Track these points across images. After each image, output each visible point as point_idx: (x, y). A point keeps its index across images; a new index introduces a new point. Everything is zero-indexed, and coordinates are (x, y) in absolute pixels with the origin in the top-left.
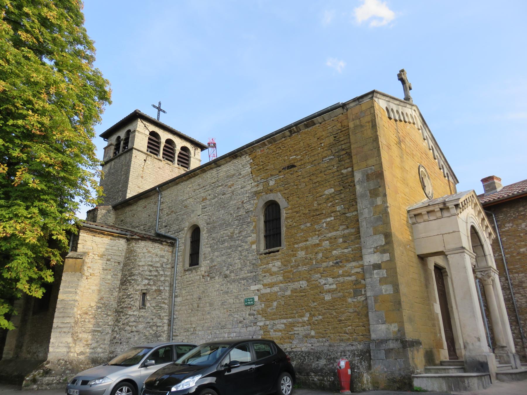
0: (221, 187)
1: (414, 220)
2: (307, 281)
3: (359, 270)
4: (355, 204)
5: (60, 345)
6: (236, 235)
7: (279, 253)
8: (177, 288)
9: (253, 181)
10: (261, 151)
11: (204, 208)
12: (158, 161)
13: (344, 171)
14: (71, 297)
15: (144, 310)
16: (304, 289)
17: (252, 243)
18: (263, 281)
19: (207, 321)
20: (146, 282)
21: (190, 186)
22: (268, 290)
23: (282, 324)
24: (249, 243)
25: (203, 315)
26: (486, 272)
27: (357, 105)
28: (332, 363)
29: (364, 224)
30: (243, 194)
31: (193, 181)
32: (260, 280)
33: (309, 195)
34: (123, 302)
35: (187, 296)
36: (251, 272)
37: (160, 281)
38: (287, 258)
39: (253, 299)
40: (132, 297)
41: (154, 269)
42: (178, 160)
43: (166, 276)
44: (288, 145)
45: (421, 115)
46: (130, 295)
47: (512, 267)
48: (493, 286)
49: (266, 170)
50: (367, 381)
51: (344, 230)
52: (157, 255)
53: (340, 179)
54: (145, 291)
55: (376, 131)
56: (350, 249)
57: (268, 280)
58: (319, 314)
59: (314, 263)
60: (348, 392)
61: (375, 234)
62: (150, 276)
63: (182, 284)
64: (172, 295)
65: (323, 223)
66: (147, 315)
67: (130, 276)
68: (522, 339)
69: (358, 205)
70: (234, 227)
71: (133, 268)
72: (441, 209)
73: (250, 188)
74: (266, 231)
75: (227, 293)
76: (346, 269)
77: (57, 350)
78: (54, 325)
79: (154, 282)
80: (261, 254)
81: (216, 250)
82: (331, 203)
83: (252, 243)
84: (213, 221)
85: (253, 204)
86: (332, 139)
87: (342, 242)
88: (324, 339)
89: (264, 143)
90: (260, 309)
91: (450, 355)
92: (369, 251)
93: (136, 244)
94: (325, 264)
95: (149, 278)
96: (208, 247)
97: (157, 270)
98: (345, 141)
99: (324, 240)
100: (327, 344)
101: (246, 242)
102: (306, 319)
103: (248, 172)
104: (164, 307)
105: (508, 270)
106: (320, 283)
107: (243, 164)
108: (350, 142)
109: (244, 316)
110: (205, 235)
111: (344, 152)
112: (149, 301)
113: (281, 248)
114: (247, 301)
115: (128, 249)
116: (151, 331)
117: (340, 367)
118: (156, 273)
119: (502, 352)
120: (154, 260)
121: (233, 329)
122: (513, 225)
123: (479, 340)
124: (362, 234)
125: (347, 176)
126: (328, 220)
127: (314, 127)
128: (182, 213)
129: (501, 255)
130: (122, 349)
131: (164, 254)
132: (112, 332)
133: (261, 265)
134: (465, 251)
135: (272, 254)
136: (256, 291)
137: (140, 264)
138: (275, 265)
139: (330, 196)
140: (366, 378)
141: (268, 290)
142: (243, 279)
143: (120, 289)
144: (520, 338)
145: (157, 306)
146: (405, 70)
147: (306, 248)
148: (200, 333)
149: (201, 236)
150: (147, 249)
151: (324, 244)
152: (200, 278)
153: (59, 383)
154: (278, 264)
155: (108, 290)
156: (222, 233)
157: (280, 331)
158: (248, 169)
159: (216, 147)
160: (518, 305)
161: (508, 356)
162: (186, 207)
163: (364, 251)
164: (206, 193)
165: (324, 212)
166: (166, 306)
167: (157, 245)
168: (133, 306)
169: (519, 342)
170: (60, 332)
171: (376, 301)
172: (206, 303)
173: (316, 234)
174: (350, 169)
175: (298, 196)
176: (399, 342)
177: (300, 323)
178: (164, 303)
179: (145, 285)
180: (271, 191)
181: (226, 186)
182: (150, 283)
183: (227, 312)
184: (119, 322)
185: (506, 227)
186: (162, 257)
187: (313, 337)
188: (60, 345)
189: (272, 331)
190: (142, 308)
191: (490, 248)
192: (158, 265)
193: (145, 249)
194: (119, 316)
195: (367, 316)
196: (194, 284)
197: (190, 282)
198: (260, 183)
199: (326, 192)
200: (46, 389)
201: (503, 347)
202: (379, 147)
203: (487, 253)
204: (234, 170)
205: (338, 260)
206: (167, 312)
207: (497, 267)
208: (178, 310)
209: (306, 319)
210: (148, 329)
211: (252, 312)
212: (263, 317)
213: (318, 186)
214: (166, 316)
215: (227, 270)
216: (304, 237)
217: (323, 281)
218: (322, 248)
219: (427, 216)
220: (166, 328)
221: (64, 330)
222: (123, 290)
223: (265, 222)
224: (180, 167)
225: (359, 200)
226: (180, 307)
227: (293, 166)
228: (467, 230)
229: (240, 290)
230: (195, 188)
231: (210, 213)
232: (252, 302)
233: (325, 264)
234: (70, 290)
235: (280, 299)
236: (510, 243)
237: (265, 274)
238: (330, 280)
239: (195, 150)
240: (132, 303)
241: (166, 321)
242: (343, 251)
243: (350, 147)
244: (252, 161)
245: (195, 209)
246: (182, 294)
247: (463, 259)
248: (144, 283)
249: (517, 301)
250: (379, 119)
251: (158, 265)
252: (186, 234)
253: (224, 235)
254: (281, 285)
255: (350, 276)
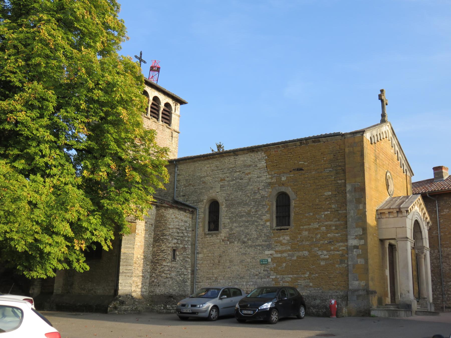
0: (238, 173)
1: (380, 216)
2: (308, 251)
3: (344, 248)
4: (345, 205)
5: (126, 284)
6: (253, 212)
7: (288, 230)
8: (199, 247)
9: (267, 174)
10: (275, 152)
11: (222, 187)
12: (147, 119)
13: (339, 182)
14: (130, 251)
15: (175, 263)
16: (306, 257)
17: (267, 221)
18: (275, 248)
19: (228, 273)
20: (176, 241)
21: (208, 166)
22: (279, 255)
23: (289, 278)
24: (264, 220)
25: (223, 268)
26: (421, 250)
27: (352, 136)
28: (324, 302)
29: (350, 220)
30: (259, 182)
31: (210, 162)
32: (272, 248)
33: (313, 193)
34: (158, 256)
35: (208, 254)
36: (266, 242)
37: (185, 241)
38: (294, 235)
39: (267, 260)
40: (165, 252)
41: (181, 231)
42: (162, 117)
43: (189, 237)
44: (298, 153)
45: (392, 128)
46: (163, 250)
47: (444, 243)
48: (425, 259)
49: (279, 167)
50: (345, 312)
51: (336, 221)
52: (182, 221)
53: (336, 187)
54: (175, 248)
55: (363, 159)
56: (340, 234)
57: (280, 248)
58: (316, 273)
59: (315, 240)
60: (335, 317)
61: (356, 227)
62: (178, 236)
63: (203, 244)
64: (194, 253)
65: (322, 215)
66: (177, 266)
67: (162, 236)
68: (442, 295)
69: (347, 207)
70: (251, 206)
71: (164, 230)
72: (397, 212)
73: (265, 179)
74: (277, 212)
75: (245, 254)
76: (336, 246)
77: (124, 288)
78: (121, 271)
79: (181, 241)
80: (274, 230)
81: (236, 222)
82: (328, 202)
83: (267, 221)
84: (232, 199)
85: (268, 192)
86: (332, 156)
87: (335, 229)
88: (319, 289)
89: (279, 146)
90: (273, 267)
91: (391, 302)
92: (352, 237)
93: (165, 210)
94: (322, 242)
95: (178, 238)
96: (227, 219)
97: (183, 233)
98: (342, 160)
99: (322, 226)
100: (320, 291)
101: (262, 220)
102: (307, 275)
103: (264, 166)
104: (188, 261)
105: (441, 244)
106: (317, 253)
107: (259, 158)
108: (345, 162)
109: (259, 271)
110: (224, 209)
111: (340, 168)
112: (178, 256)
113: (290, 227)
114: (262, 262)
115: (157, 214)
116: (180, 278)
117: (332, 304)
118: (182, 235)
119: (423, 301)
120: (180, 224)
121: (251, 280)
122: (449, 211)
123: (409, 292)
124: (348, 226)
125: (341, 185)
126: (326, 213)
127: (319, 143)
128: (201, 187)
129: (438, 233)
130: (160, 290)
131: (187, 220)
132: (150, 277)
133: (274, 238)
134: (408, 240)
135: (282, 231)
136: (270, 255)
137: (170, 227)
138: (285, 239)
139: (328, 197)
140: (345, 310)
141: (279, 255)
142: (259, 245)
143: (153, 245)
144: (441, 295)
145: (184, 259)
146: (384, 90)
147: (309, 230)
148: (221, 281)
149: (220, 209)
150: (175, 216)
151: (322, 229)
152: (220, 241)
153: (132, 310)
154: (288, 238)
155: (146, 246)
156: (240, 209)
157: (288, 282)
158: (263, 164)
159: (159, 72)
160: (444, 271)
161: (427, 304)
162: (204, 182)
163: (349, 237)
164: (224, 175)
165: (323, 207)
166: (190, 260)
167: (182, 212)
168: (167, 259)
169: (440, 297)
170: (125, 276)
171: (354, 268)
172: (226, 260)
173: (316, 222)
174: (343, 181)
175: (304, 192)
176: (365, 291)
177: (303, 278)
178: (188, 258)
179: (174, 244)
180: (283, 184)
181: (243, 173)
182: (179, 242)
183: (245, 267)
184: (156, 270)
185: (444, 212)
186: (186, 222)
187: (311, 287)
188: (126, 284)
189: (282, 282)
190: (174, 261)
191: (427, 232)
192: (183, 228)
193: (173, 215)
194: (155, 266)
195: (347, 275)
196: (215, 246)
197: (211, 244)
198: (274, 177)
199: (326, 194)
200: (124, 314)
201: (425, 298)
202: (364, 171)
203: (424, 237)
204: (251, 161)
205: (331, 240)
206: (190, 264)
207: (430, 247)
208: (200, 263)
209: (307, 275)
210: (178, 276)
211: (266, 269)
212: (274, 272)
213: (320, 188)
214: (189, 267)
215: (245, 238)
216: (308, 222)
217: (320, 253)
218: (321, 231)
219: (388, 215)
220: (190, 276)
221: (128, 274)
222: (157, 246)
223: (277, 206)
224: (164, 124)
225: (348, 204)
226: (202, 262)
227: (301, 169)
228: (411, 225)
229: (256, 253)
230: (213, 168)
231: (228, 192)
232: (266, 262)
233: (322, 242)
234: (129, 246)
235: (288, 262)
236: (445, 225)
237: (277, 244)
238: (325, 252)
239: (175, 105)
240: (165, 256)
241: (189, 271)
242: (335, 235)
243: (345, 165)
244: (267, 157)
245: (214, 187)
246: (203, 252)
247: (406, 244)
248: (174, 242)
249: (444, 268)
250: (366, 149)
251: (183, 228)
252: (205, 206)
253: (242, 211)
254: (290, 253)
255: (339, 251)
